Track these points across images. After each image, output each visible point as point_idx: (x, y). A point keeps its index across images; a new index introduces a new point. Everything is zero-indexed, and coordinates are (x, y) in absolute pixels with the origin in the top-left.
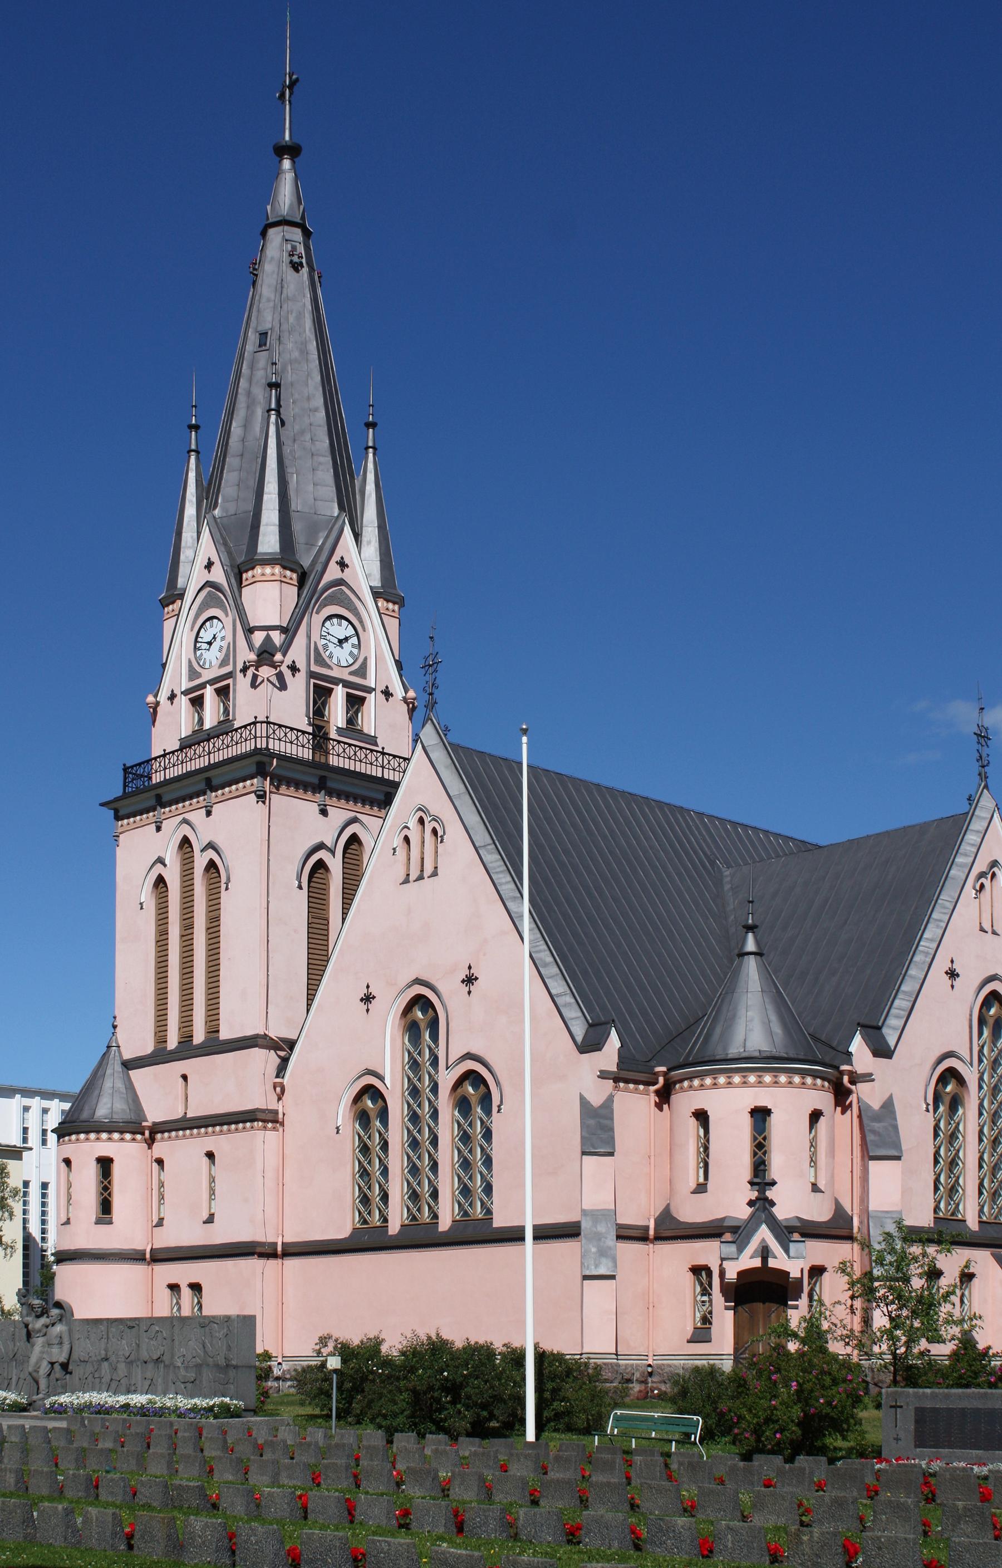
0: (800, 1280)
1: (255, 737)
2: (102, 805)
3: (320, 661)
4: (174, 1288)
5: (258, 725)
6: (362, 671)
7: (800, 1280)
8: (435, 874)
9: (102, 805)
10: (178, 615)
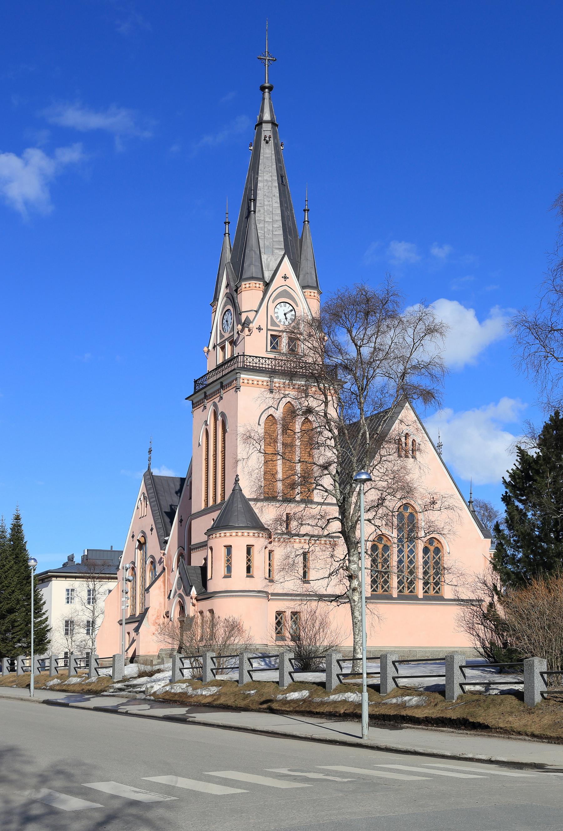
2: (186, 399)
3: (274, 323)
9: (186, 399)
10: (216, 311)
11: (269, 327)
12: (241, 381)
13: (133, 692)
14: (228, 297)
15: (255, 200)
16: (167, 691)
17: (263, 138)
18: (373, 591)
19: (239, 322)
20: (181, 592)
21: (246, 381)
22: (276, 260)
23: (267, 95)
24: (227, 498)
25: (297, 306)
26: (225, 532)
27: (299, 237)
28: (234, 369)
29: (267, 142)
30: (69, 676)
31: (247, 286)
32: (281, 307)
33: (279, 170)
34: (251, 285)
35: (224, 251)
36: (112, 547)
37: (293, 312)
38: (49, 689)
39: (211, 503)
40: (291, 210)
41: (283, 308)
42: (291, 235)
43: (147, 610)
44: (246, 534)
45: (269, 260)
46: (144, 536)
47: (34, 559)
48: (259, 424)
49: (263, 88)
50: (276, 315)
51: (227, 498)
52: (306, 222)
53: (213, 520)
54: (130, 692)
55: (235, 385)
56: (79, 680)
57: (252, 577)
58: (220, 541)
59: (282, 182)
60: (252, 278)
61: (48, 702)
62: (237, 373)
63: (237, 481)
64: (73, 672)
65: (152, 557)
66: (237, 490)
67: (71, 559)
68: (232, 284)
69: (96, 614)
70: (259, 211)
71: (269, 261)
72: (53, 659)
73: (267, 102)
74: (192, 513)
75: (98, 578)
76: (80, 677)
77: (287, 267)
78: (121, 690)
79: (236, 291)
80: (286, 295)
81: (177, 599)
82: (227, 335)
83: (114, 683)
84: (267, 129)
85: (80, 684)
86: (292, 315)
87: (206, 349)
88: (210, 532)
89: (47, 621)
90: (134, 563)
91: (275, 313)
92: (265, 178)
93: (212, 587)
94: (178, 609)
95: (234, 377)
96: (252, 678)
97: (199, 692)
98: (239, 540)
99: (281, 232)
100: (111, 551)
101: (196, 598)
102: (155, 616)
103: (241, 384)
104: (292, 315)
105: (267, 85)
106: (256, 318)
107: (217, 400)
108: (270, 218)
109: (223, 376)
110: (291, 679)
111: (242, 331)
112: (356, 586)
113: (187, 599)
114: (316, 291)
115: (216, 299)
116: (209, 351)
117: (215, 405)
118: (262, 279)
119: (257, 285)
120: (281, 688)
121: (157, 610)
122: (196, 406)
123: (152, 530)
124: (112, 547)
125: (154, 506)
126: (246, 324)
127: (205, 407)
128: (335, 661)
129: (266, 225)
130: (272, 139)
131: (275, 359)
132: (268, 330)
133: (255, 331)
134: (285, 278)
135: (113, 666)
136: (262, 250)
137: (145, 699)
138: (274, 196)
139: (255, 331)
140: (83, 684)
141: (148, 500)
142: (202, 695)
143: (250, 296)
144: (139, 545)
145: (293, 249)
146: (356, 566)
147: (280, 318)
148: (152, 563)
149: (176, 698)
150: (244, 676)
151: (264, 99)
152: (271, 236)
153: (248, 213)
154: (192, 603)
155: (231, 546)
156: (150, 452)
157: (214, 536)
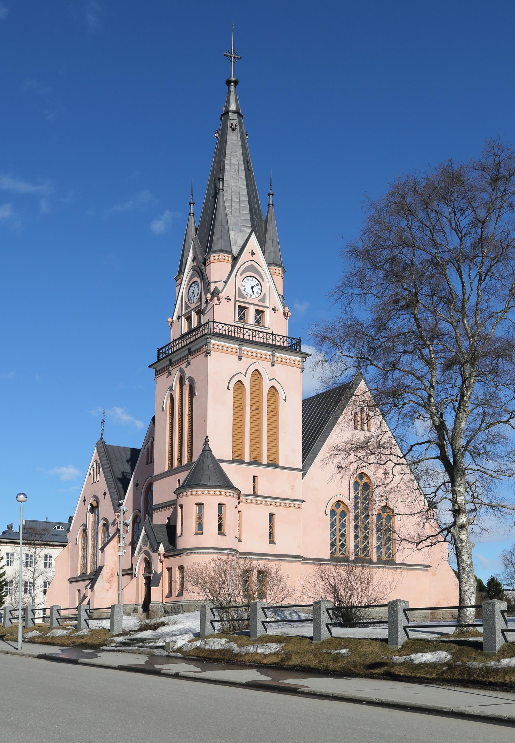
0: (19, 533)
1: (208, 328)
2: (149, 367)
3: (241, 295)
5: (210, 323)
6: (263, 300)
7: (19, 533)
9: (149, 367)
10: (181, 284)
11: (237, 299)
12: (212, 346)
13: (146, 647)
14: (194, 270)
15: (223, 179)
16: (198, 648)
17: (229, 126)
18: (331, 553)
19: (207, 291)
20: (147, 548)
21: (216, 347)
22: (243, 237)
23: (232, 88)
24: (195, 459)
25: (263, 281)
26: (197, 490)
27: (264, 219)
28: (206, 334)
29: (234, 130)
30: (50, 628)
31: (217, 258)
32: (248, 280)
33: (245, 156)
34: (220, 257)
35: (189, 229)
36: (47, 518)
37: (259, 287)
38: (28, 642)
39: (176, 464)
40: (256, 194)
41: (250, 281)
42: (256, 215)
43: (101, 568)
44: (218, 493)
45: (236, 236)
46: (97, 500)
47: (23, 494)
48: (228, 388)
49: (228, 82)
50: (243, 288)
51: (195, 459)
52: (271, 205)
53: (179, 481)
54: (142, 647)
55: (206, 350)
56: (65, 632)
57: (223, 534)
58: (190, 500)
59: (248, 167)
60: (221, 251)
61: (40, 657)
62: (207, 338)
63: (206, 442)
64: (55, 624)
65: (105, 519)
66: (206, 451)
67: (10, 527)
68: (200, 257)
69: (37, 575)
70: (227, 191)
71: (236, 238)
72: (30, 609)
73: (232, 94)
74: (155, 474)
75: (38, 544)
76: (64, 628)
77: (254, 243)
78: (124, 644)
79: (204, 263)
80: (252, 270)
81: (142, 556)
82: (193, 306)
83: (113, 636)
84: (233, 118)
85: (68, 637)
86: (258, 289)
87: (170, 320)
88: (178, 492)
89: (4, 575)
90: (85, 525)
91: (243, 285)
92: (232, 162)
93: (181, 544)
94: (143, 565)
95: (205, 343)
96: (331, 633)
97: (251, 649)
98: (211, 498)
99: (247, 211)
100: (46, 522)
101: (164, 555)
102: (109, 574)
103: (211, 349)
104: (258, 289)
105: (233, 78)
106: (225, 289)
107: (183, 366)
108: (237, 198)
109: (191, 343)
110: (405, 636)
111: (211, 299)
112: (465, 522)
113: (154, 556)
114: (281, 269)
115: (181, 272)
116: (173, 322)
117: (182, 371)
118: (230, 252)
119: (226, 258)
120: (391, 647)
121: (111, 569)
122: (160, 373)
123: (105, 494)
124: (47, 518)
125: (107, 472)
126: (216, 293)
127: (170, 374)
128: (499, 613)
129: (233, 204)
130: (238, 127)
131: (244, 328)
132: (236, 301)
133: (224, 301)
134: (252, 253)
135: (111, 618)
136: (230, 227)
137: (168, 656)
138: (241, 178)
139: (224, 301)
140: (73, 637)
141: (101, 467)
142: (257, 653)
143: (218, 269)
144: (91, 509)
145: (259, 227)
146: (462, 498)
147: (247, 291)
148: (104, 525)
149: (217, 656)
150: (322, 631)
151: (229, 92)
152: (238, 214)
153: (215, 192)
154: (160, 559)
155: (203, 504)
156: (103, 422)
157: (185, 494)
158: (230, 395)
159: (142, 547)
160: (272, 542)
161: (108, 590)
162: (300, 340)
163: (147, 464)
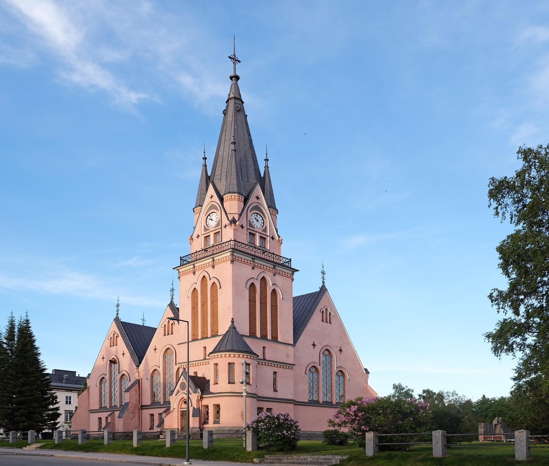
3: (251, 225)
4: (152, 415)
6: (265, 230)
8: (172, 334)
158: (247, 292)
159: (180, 390)
160: (275, 390)
161: (132, 419)
162: (291, 260)
163: (165, 335)
